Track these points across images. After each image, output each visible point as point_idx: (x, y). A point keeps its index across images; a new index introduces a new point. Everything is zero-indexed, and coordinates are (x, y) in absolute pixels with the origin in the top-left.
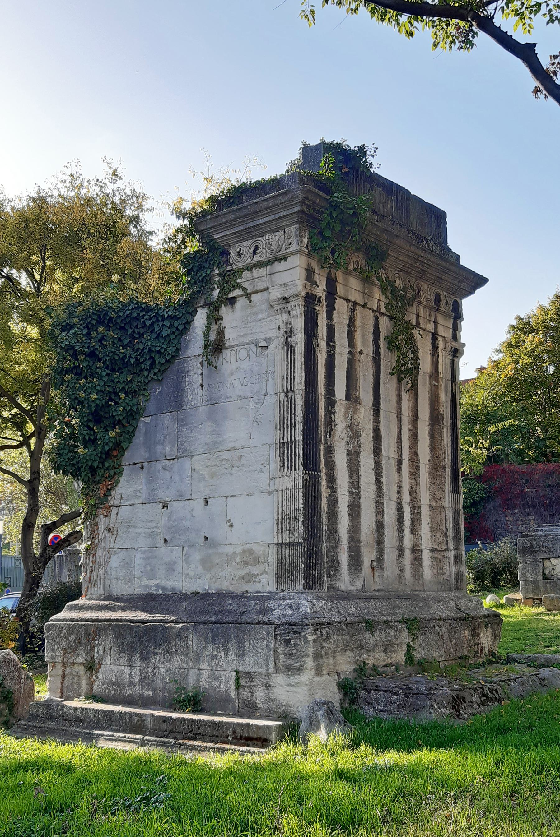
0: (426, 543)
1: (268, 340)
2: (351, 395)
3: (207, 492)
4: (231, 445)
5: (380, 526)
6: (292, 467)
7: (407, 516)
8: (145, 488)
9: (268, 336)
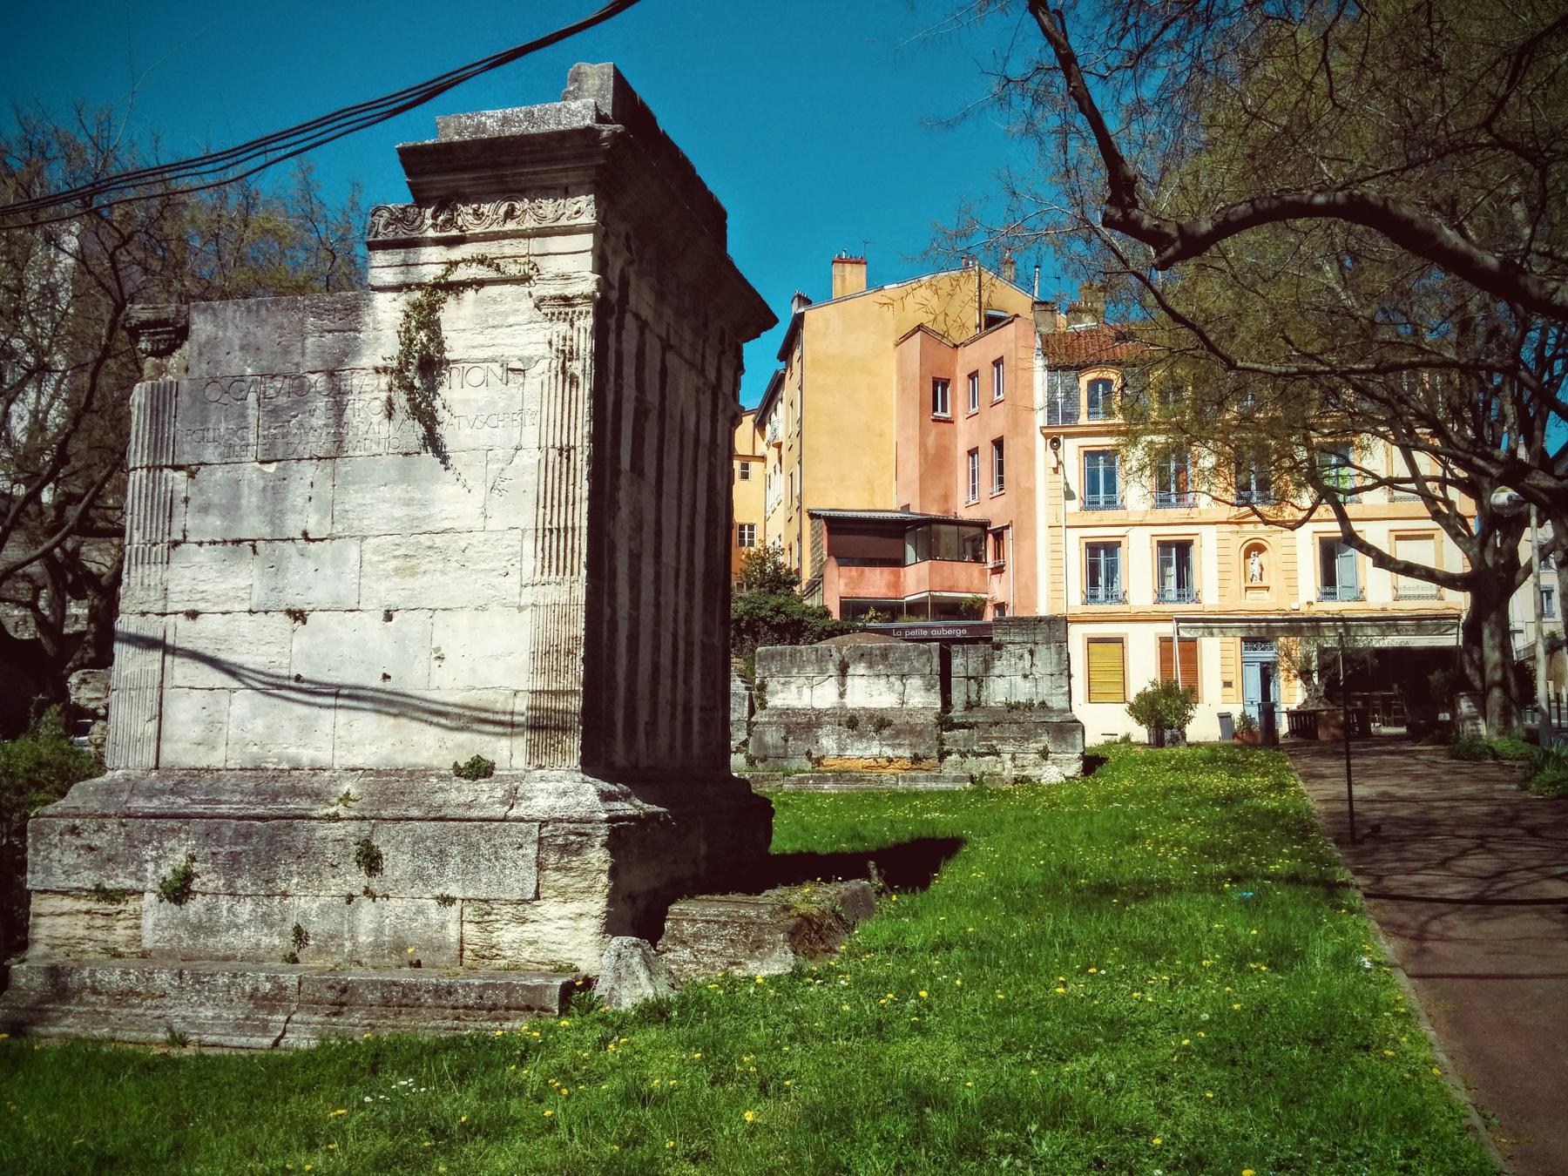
0: (697, 701)
1: (530, 361)
2: (637, 469)
3: (393, 600)
4: (446, 525)
5: (656, 667)
6: (564, 568)
7: (681, 655)
8: (257, 585)
9: (527, 353)
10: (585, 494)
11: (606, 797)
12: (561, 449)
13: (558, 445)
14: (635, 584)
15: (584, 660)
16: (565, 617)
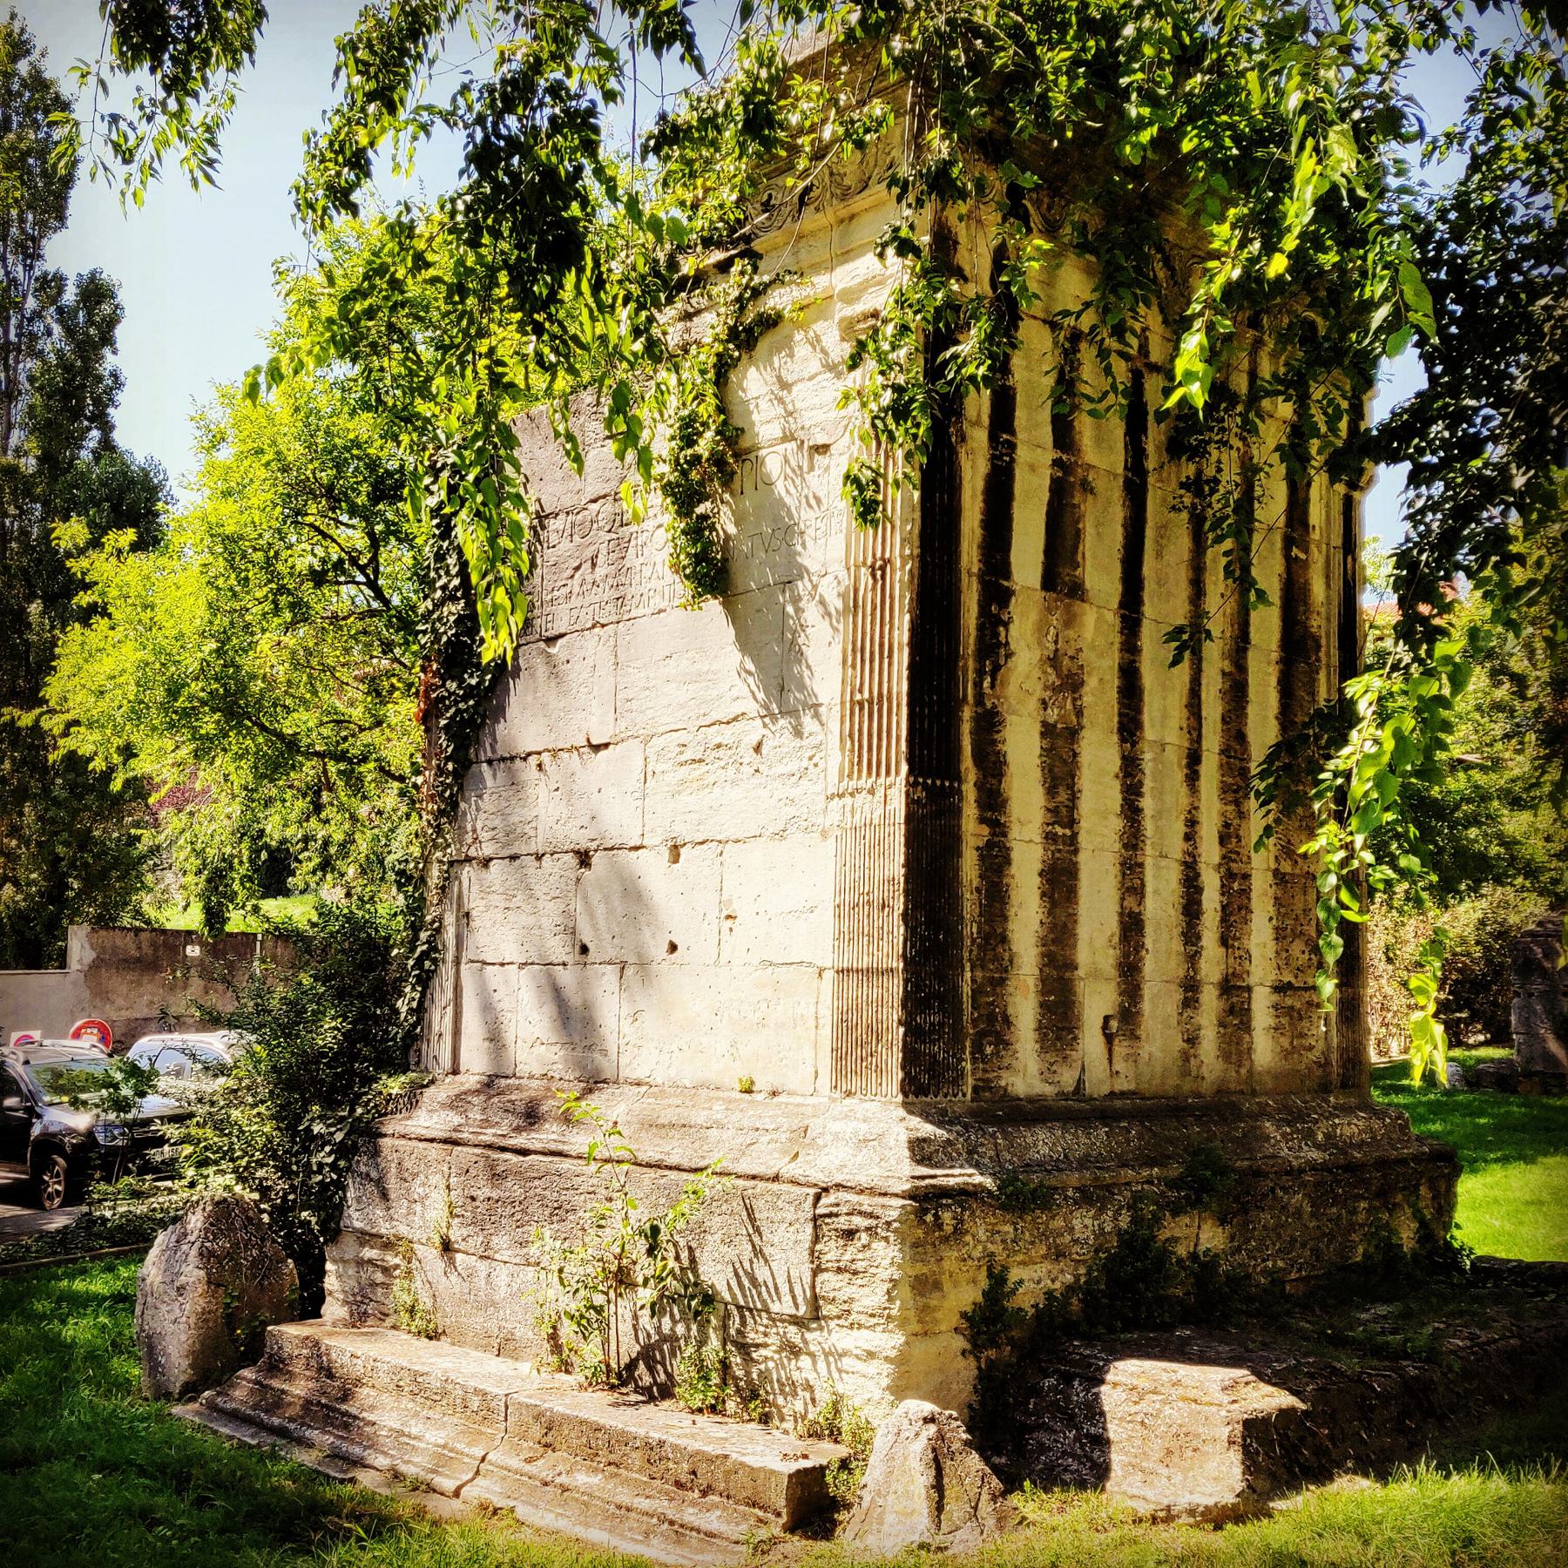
3: (684, 832)
10: (906, 638)
11: (921, 1151)
12: (873, 567)
13: (869, 561)
14: (1060, 774)
15: (905, 915)
16: (877, 848)
